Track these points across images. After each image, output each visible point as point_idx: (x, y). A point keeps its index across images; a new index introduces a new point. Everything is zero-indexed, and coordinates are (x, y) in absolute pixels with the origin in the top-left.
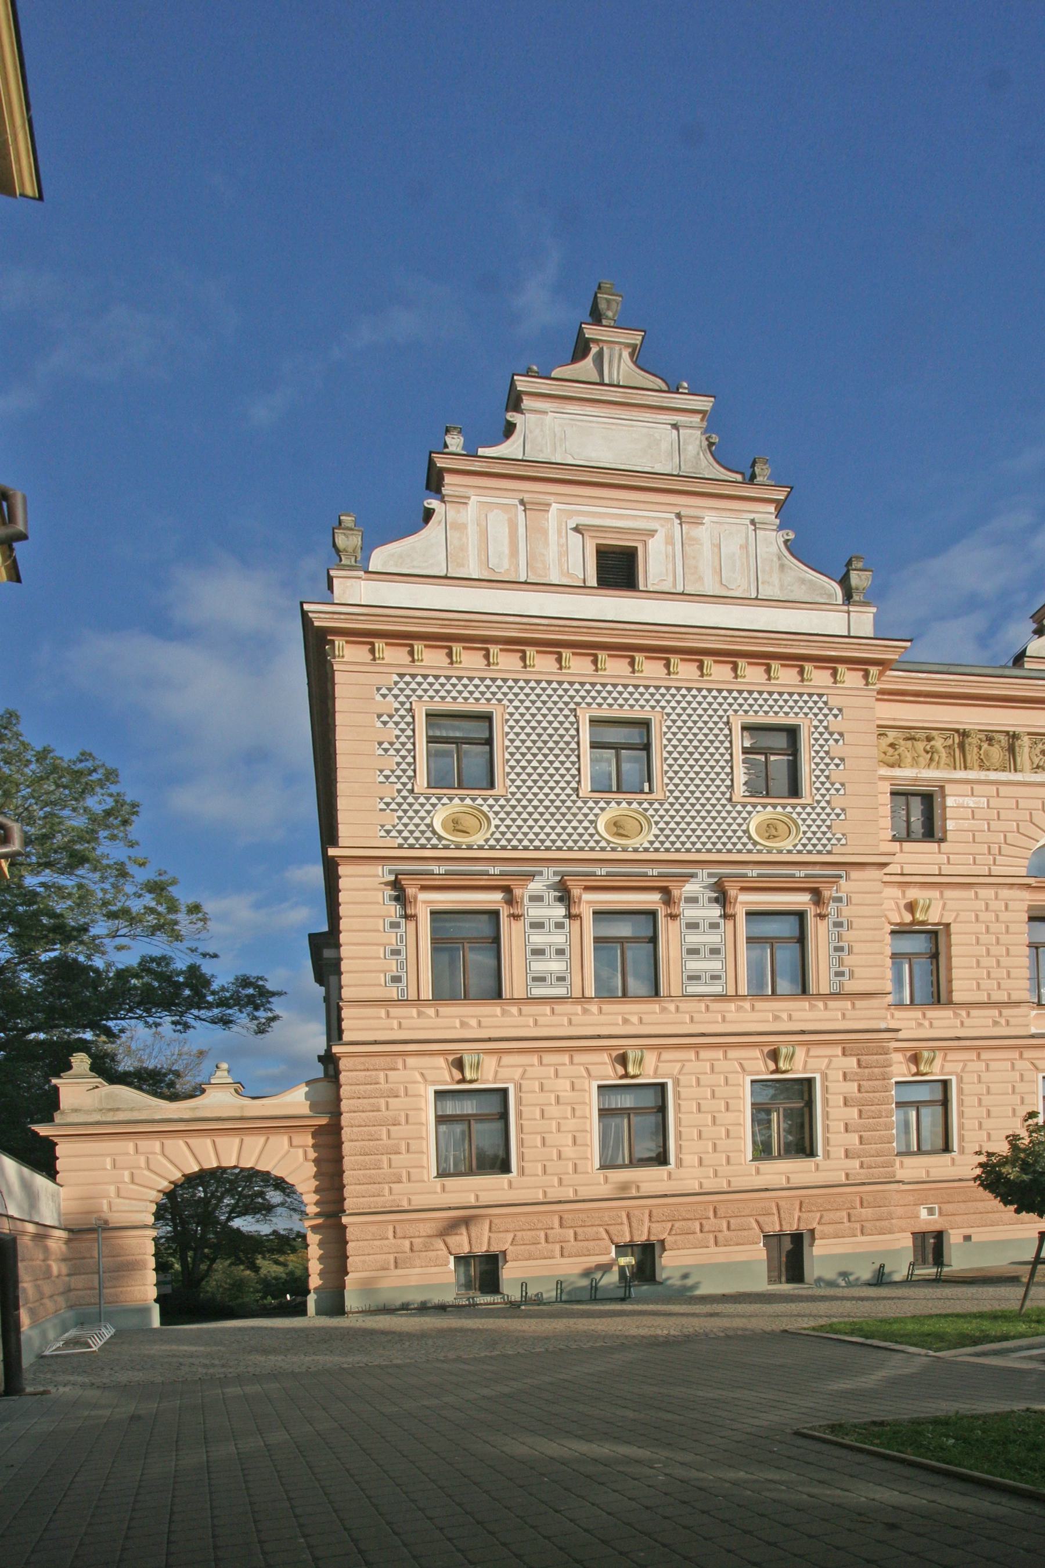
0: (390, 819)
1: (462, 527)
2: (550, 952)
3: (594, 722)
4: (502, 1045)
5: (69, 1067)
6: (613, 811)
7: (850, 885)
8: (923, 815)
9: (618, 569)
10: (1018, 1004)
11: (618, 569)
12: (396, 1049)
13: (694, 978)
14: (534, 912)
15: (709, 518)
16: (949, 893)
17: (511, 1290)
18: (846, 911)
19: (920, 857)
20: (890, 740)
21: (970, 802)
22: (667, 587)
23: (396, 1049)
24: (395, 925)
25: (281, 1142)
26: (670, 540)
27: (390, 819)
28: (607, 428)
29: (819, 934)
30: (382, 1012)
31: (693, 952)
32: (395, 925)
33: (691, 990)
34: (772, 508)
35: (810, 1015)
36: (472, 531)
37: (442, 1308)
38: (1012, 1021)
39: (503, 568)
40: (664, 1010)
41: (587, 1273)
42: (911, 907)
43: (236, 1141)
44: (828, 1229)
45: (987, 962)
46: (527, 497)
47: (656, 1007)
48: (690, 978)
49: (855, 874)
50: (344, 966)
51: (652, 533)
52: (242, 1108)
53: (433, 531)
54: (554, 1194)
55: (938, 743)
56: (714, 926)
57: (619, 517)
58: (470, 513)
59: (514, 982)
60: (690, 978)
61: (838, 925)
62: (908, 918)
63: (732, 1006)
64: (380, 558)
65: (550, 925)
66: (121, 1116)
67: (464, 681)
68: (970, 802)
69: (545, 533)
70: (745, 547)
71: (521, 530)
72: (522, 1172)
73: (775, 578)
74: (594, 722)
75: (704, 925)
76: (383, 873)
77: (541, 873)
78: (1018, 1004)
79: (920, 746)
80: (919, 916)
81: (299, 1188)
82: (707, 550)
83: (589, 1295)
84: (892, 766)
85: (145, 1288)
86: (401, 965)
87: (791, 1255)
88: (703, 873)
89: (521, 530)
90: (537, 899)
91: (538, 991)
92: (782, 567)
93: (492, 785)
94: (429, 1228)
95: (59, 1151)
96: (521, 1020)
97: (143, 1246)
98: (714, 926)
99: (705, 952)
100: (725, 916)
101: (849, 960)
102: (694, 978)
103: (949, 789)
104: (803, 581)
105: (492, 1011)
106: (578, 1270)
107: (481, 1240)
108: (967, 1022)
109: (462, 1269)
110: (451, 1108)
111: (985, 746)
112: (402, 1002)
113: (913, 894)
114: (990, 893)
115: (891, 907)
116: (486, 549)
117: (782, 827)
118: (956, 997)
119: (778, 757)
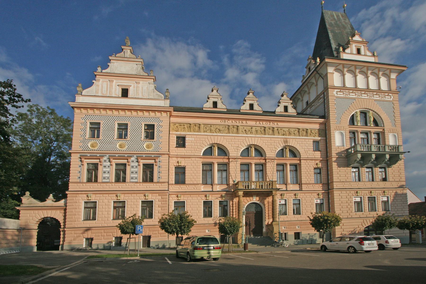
0: (81, 144)
1: (98, 86)
2: (107, 172)
3: (91, 123)
4: (96, 192)
5: (25, 194)
6: (120, 142)
7: (162, 158)
8: (181, 142)
9: (125, 93)
10: (198, 184)
11: (125, 93)
12: (78, 192)
13: (132, 178)
14: (132, 164)
15: (141, 82)
16: (186, 159)
17: (94, 247)
18: (161, 164)
19: (181, 151)
20: (177, 126)
21: (191, 139)
22: (133, 97)
23: (78, 192)
24: (80, 166)
25: (58, 212)
26: (134, 87)
27: (81, 144)
28: (125, 64)
29: (156, 169)
30: (76, 185)
31: (132, 172)
32: (80, 166)
33: (132, 181)
34: (153, 80)
35: (153, 187)
36: (100, 86)
37: (79, 250)
38: (197, 188)
39: (105, 93)
40: (126, 185)
41: (108, 243)
42: (178, 162)
43: (50, 211)
44: (154, 235)
45: (308, 177)
46: (110, 79)
47: (125, 184)
48: (132, 178)
49: (163, 156)
50: (71, 175)
51: (131, 86)
52: (52, 204)
53: (93, 87)
54: (103, 225)
55: (186, 126)
56: (136, 167)
57: (125, 83)
58: (100, 82)
59: (100, 179)
60: (132, 178)
61: (159, 167)
62: (178, 165)
63: (139, 184)
64: (84, 92)
65: (107, 167)
66: (32, 205)
67: (96, 116)
68: (191, 139)
69: (112, 86)
70: (147, 88)
71: (109, 86)
72: (98, 220)
73: (152, 94)
74: (91, 123)
75: (135, 167)
76: (79, 155)
77: (134, 156)
78: (198, 184)
79: (182, 127)
80: (318, 166)
81: (60, 222)
82: (140, 88)
83: (108, 248)
84: (177, 131)
85: (34, 242)
86: (81, 175)
87: (90, 241)
88: (135, 156)
89: (109, 86)
90: (133, 161)
91: (104, 181)
92: (154, 92)
93: (153, 139)
94: (82, 231)
95: (21, 212)
96: (115, 187)
97: (35, 234)
98: (136, 167)
99: (134, 173)
100: (138, 165)
101: (161, 175)
102: (132, 178)
103: (187, 136)
104: (157, 94)
105: (96, 184)
106: (106, 242)
107: (89, 235)
108: (188, 188)
109: (88, 241)
110: (116, 205)
111: (194, 127)
112: (80, 183)
113: (179, 159)
114: (194, 159)
115: (174, 162)
116: (102, 91)
117: (150, 146)
118: (186, 182)
119: (150, 131)
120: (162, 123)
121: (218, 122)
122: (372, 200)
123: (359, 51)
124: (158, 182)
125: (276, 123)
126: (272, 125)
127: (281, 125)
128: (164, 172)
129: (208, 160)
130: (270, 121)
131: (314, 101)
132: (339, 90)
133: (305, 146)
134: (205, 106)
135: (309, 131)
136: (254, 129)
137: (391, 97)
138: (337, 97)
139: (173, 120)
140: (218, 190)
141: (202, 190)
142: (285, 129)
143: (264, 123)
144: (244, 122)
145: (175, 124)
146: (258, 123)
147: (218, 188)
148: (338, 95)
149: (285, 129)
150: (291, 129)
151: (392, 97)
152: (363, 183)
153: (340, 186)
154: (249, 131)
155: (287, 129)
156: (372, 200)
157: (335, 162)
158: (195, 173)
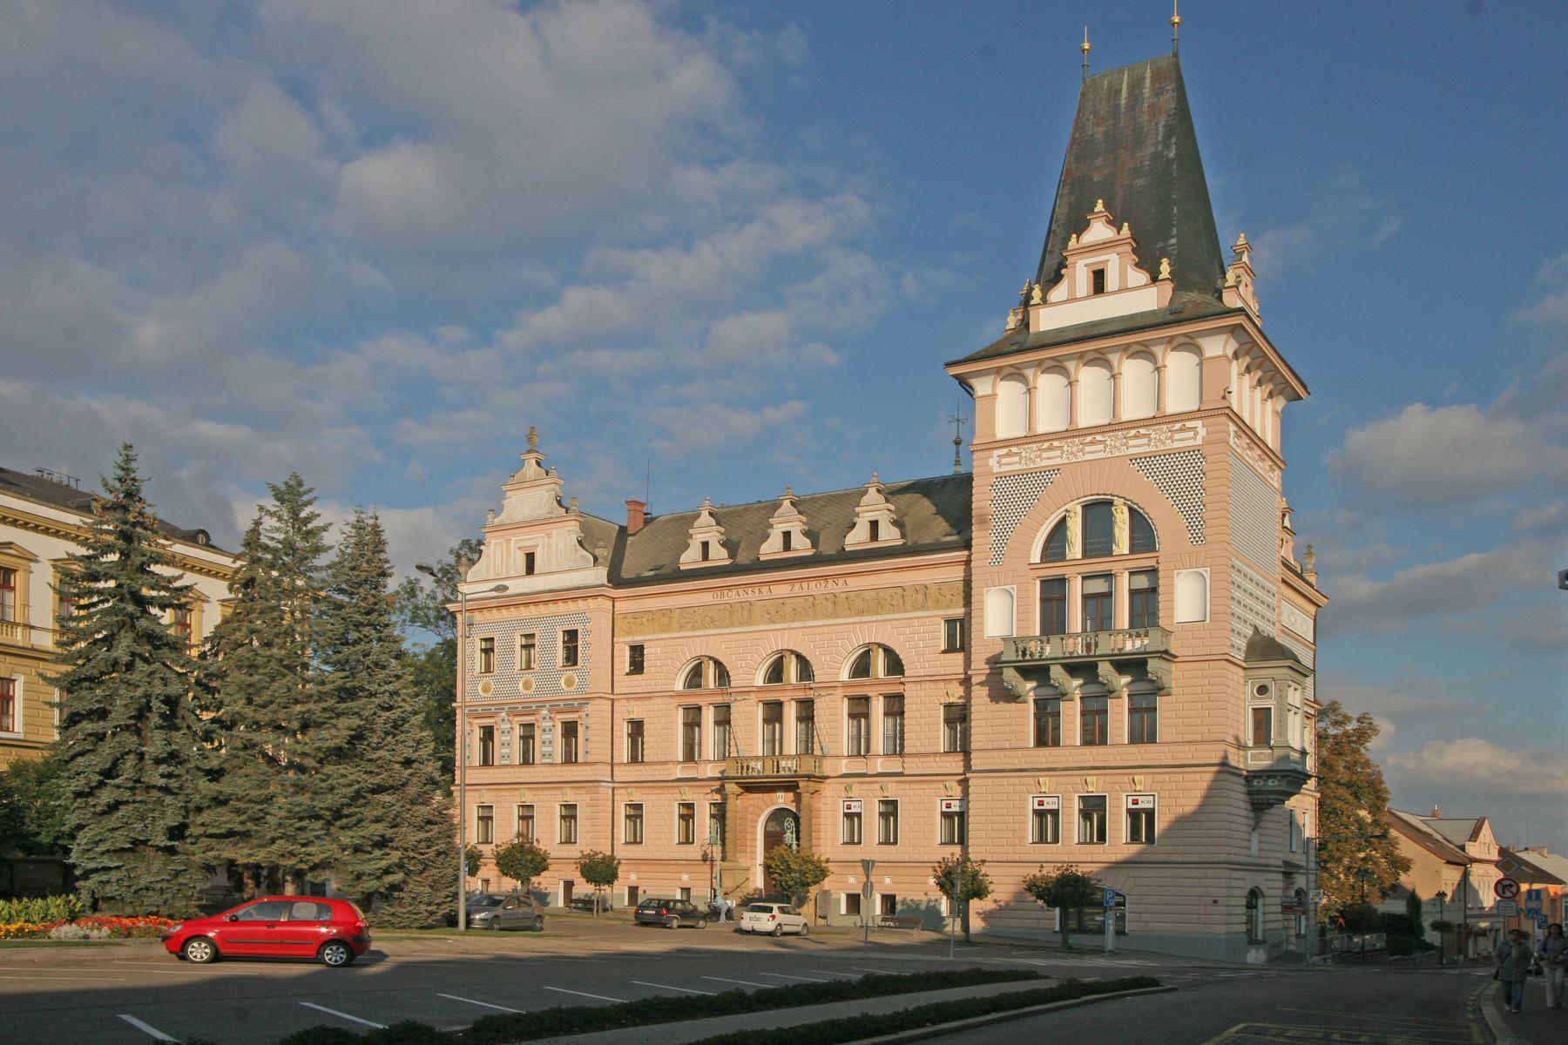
15: (555, 533)
18: (590, 720)
22: (547, 569)
120: (594, 620)
121: (706, 598)
122: (1093, 808)
123: (1099, 281)
124: (585, 763)
125: (841, 581)
126: (831, 587)
127: (854, 583)
128: (601, 737)
129: (1053, 571)
130: (826, 577)
131: (95, 945)
132: (1005, 451)
133: (919, 639)
134: (683, 559)
135: (933, 591)
136: (788, 607)
137: (1196, 434)
138: (1000, 477)
139: (621, 607)
140: (710, 775)
141: (679, 776)
142: (866, 595)
143: (812, 584)
144: (765, 589)
145: (624, 616)
146: (797, 586)
147: (710, 771)
148: (1005, 468)
149: (866, 595)
150: (881, 593)
151: (1202, 432)
152: (1114, 750)
153: (997, 761)
154: (777, 613)
155: (873, 593)
156: (1093, 808)
157: (982, 684)
158: (666, 737)
